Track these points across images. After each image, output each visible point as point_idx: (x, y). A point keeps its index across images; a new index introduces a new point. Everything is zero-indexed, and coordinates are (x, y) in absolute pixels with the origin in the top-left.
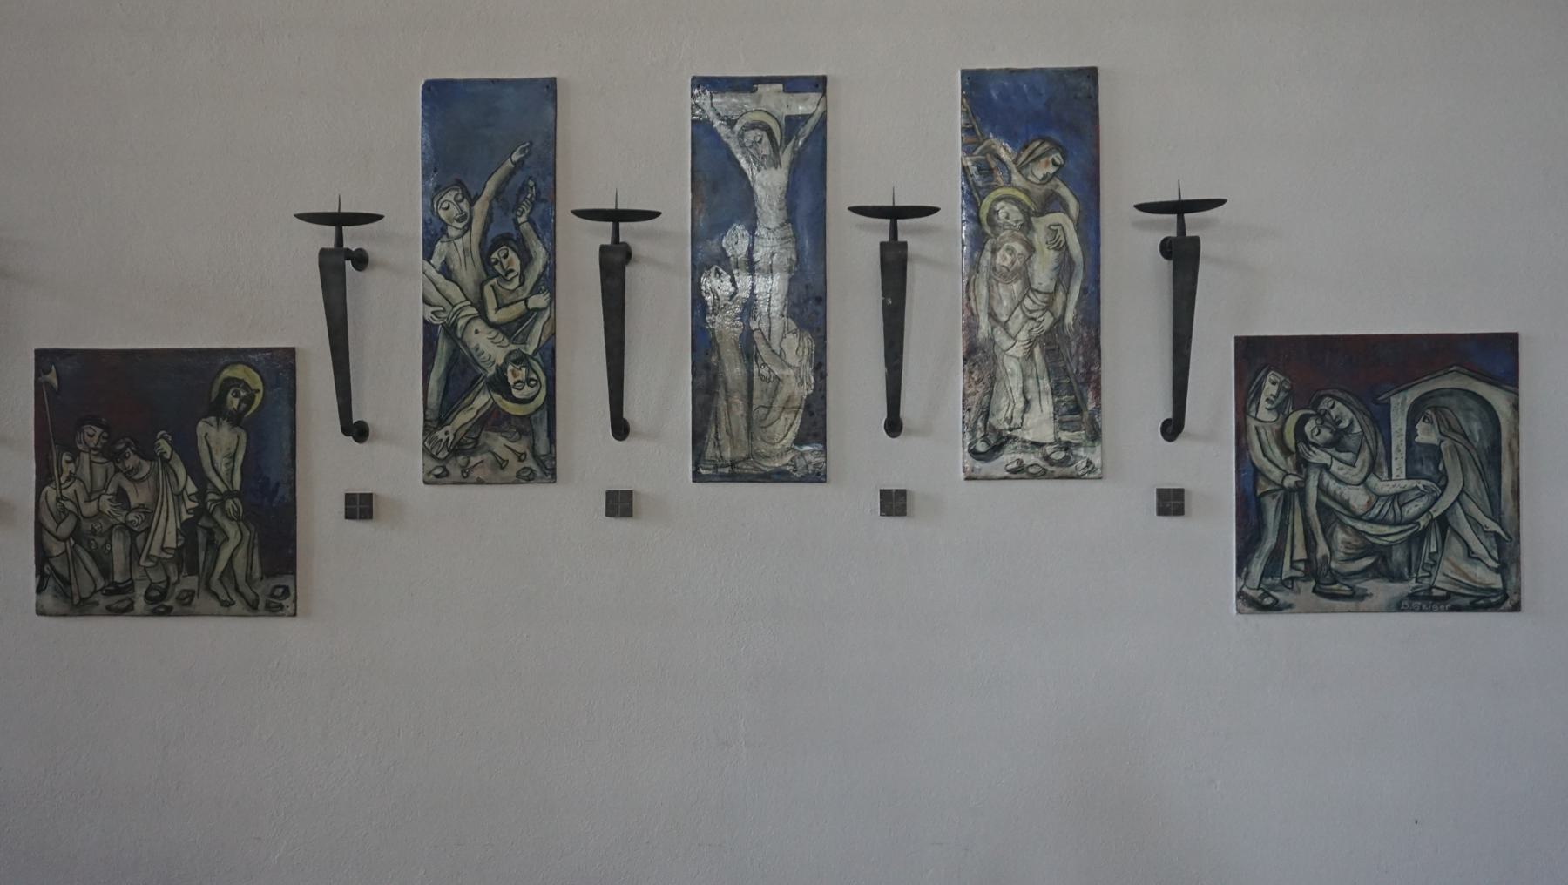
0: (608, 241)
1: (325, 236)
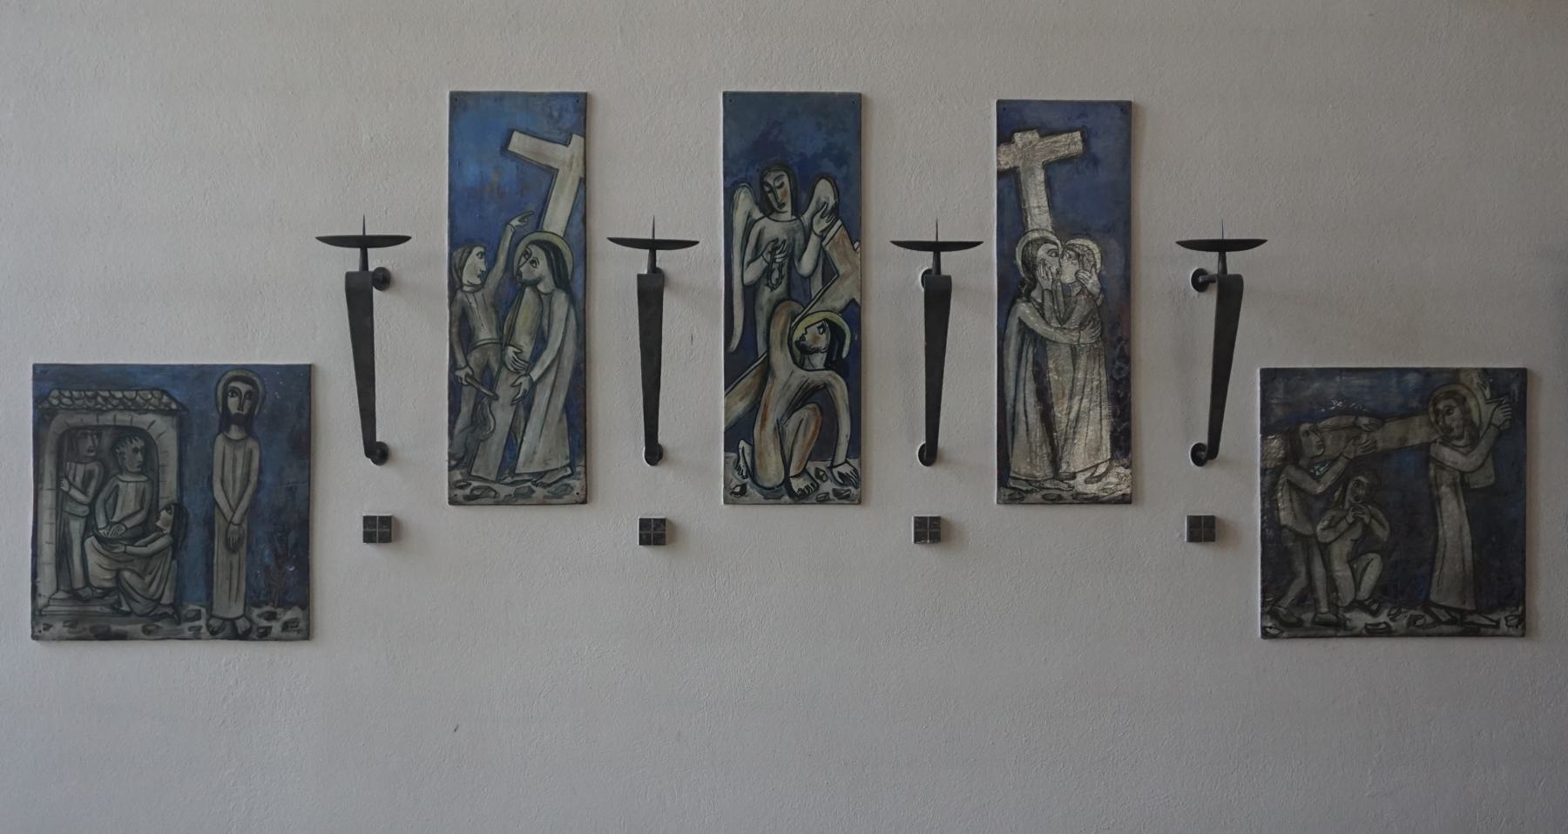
0: (355, 267)
1: (350, 259)
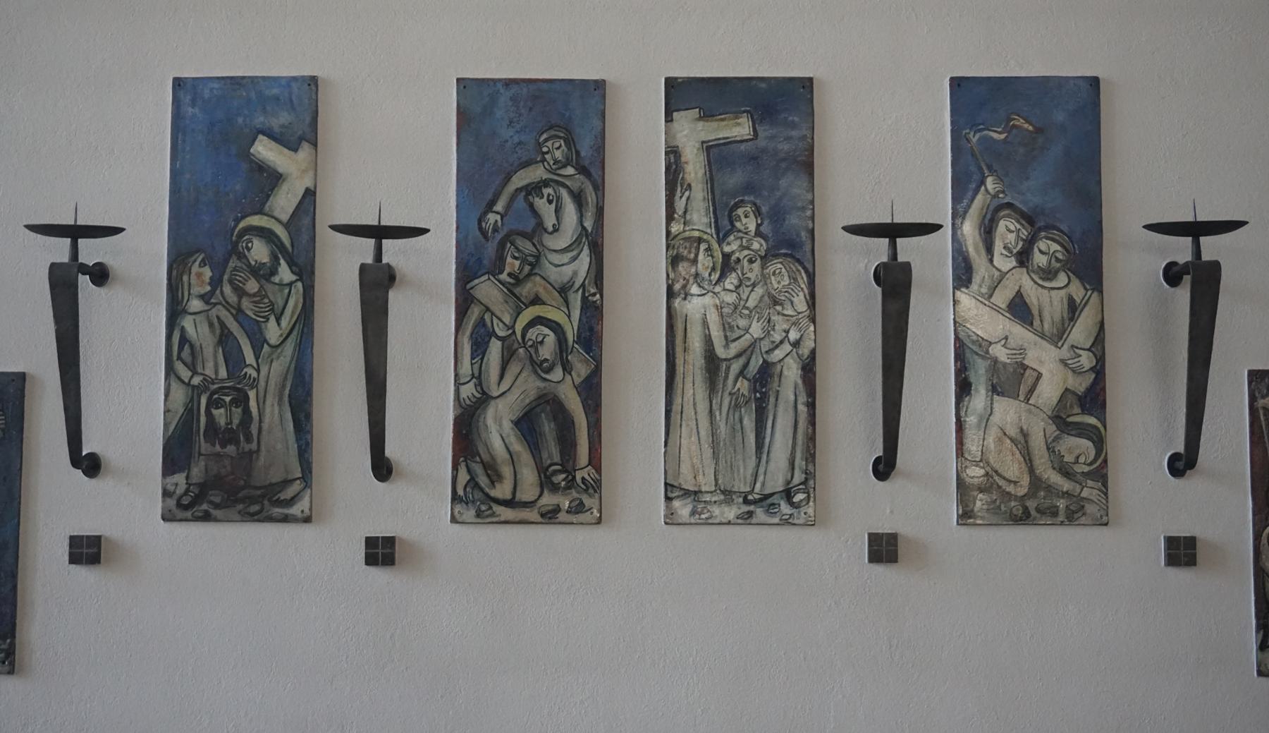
1: (59, 250)
